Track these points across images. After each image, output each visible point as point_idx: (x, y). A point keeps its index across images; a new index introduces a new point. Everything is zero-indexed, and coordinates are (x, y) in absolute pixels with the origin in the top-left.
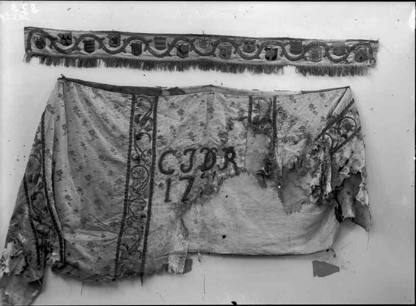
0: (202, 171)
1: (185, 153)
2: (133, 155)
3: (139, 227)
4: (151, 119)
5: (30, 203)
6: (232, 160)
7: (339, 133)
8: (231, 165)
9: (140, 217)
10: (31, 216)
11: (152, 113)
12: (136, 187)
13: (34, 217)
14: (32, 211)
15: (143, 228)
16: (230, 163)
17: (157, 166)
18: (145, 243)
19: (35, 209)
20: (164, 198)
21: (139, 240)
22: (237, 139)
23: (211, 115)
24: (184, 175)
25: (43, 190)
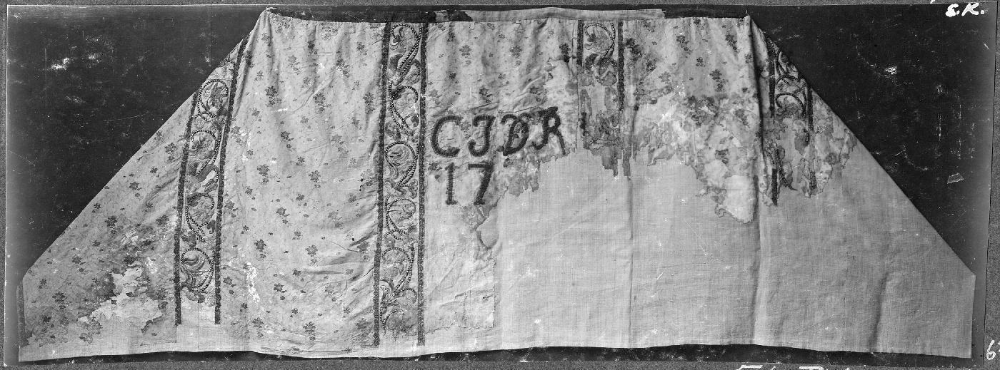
0: (505, 155)
1: (476, 123)
2: (387, 124)
3: (406, 248)
4: (416, 61)
5: (184, 210)
6: (555, 130)
7: (792, 78)
8: (554, 139)
9: (406, 231)
10: (179, 231)
11: (419, 52)
12: (396, 181)
13: (185, 234)
14: (185, 225)
15: (413, 249)
16: (551, 135)
17: (428, 141)
18: (421, 275)
19: (191, 222)
20: (445, 198)
21: (410, 269)
22: (563, 93)
23: (467, 59)
24: (475, 160)
25: (215, 193)
